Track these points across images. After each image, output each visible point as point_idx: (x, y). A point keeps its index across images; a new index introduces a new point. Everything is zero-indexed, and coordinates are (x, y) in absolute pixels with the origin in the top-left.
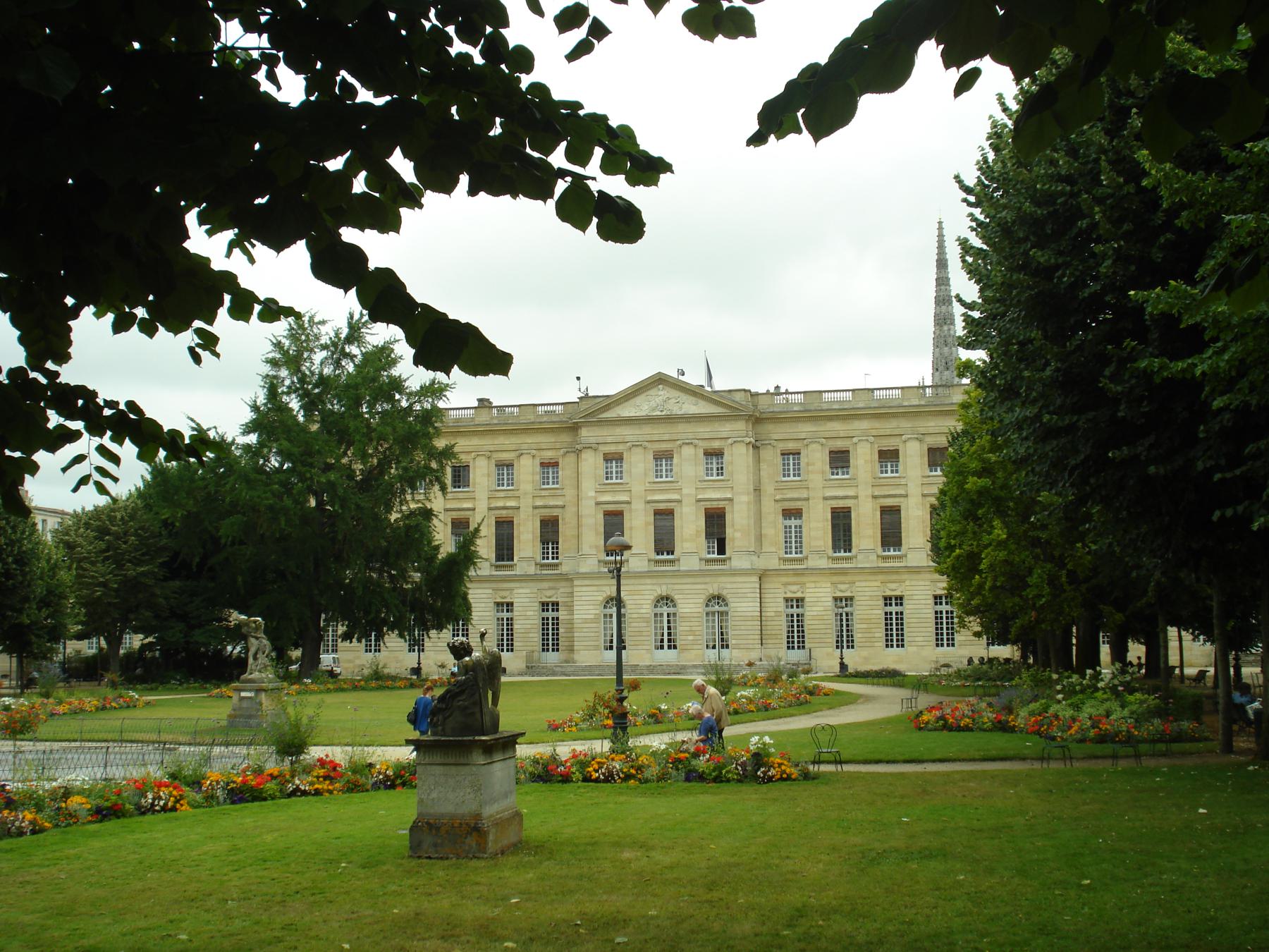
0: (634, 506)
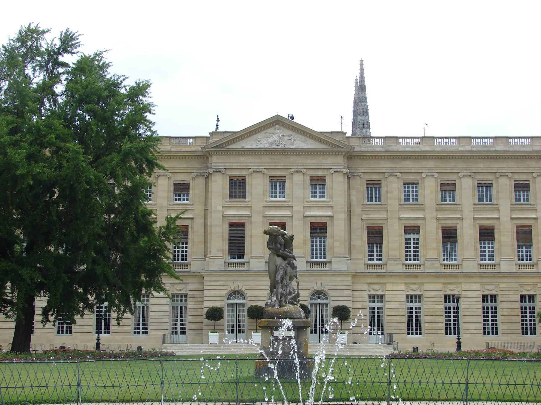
0: (254, 219)
